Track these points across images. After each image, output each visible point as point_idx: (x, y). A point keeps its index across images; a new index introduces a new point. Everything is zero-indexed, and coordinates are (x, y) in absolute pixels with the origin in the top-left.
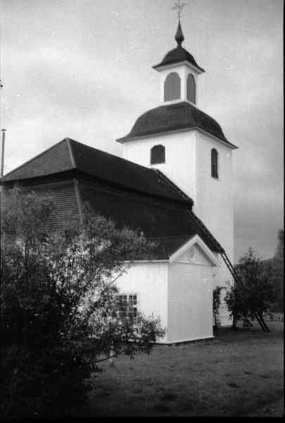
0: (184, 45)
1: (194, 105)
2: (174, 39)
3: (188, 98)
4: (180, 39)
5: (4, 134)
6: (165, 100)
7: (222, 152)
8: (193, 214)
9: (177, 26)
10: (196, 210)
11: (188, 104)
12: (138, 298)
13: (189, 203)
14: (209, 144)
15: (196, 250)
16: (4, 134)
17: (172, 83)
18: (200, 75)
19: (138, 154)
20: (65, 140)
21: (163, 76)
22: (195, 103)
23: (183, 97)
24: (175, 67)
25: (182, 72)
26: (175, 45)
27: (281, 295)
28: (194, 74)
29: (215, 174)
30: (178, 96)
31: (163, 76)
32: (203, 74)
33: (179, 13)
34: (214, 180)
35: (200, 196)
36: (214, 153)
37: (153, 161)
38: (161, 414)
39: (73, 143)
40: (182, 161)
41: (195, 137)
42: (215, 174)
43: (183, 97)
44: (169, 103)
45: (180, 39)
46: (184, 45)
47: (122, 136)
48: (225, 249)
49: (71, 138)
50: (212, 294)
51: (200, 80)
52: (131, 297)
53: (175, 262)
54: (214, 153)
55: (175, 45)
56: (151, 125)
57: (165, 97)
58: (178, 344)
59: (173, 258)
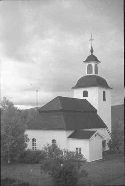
0: (94, 54)
3: (95, 73)
4: (92, 51)
5: (37, 92)
8: (97, 115)
9: (91, 47)
10: (98, 113)
11: (95, 75)
13: (96, 111)
14: (102, 90)
15: (97, 135)
16: (37, 92)
17: (90, 68)
18: (99, 64)
19: (78, 94)
20: (57, 97)
21: (86, 65)
23: (93, 73)
25: (93, 64)
28: (97, 64)
29: (104, 100)
31: (86, 65)
32: (100, 63)
33: (92, 42)
34: (105, 102)
35: (99, 107)
36: (104, 93)
38: (88, 185)
40: (94, 96)
41: (97, 89)
42: (104, 100)
43: (93, 73)
44: (88, 75)
45: (92, 51)
48: (107, 126)
49: (59, 96)
50: (102, 153)
51: (99, 66)
52: (79, 149)
53: (91, 140)
54: (104, 93)
55: (90, 54)
58: (92, 162)
59: (90, 139)
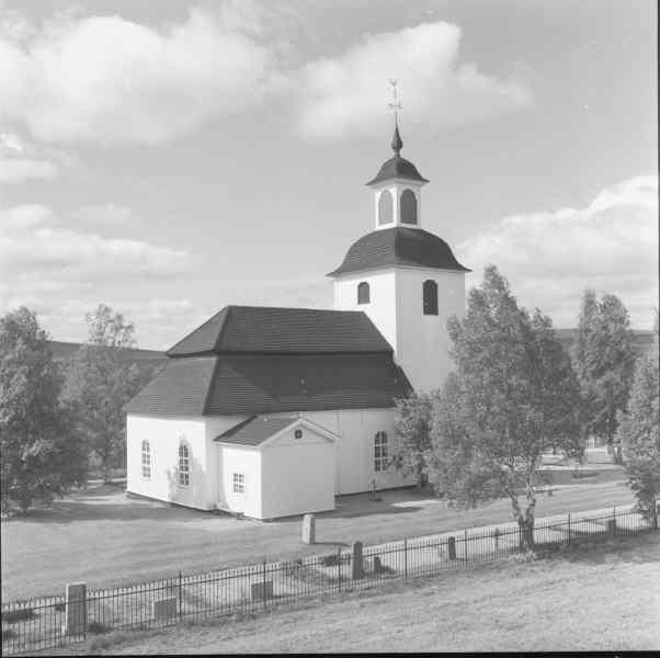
2: (390, 148)
4: (398, 145)
6: (381, 223)
19: (343, 297)
26: (392, 154)
30: (392, 221)
34: (431, 318)
55: (392, 154)
56: (363, 257)
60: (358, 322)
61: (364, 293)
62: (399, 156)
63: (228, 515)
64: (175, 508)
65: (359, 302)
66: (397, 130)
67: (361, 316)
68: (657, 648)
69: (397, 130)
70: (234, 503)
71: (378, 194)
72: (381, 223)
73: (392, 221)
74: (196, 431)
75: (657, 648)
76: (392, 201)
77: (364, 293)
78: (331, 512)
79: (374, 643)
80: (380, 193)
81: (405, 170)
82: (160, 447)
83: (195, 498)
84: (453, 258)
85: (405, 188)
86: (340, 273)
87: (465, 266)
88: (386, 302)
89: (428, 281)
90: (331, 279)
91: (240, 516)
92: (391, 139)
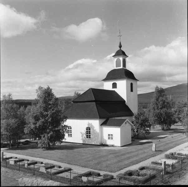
1: (125, 68)
2: (119, 47)
4: (120, 47)
6: (116, 67)
7: (133, 82)
12: (109, 134)
19: (108, 86)
20: (90, 89)
22: (125, 67)
24: (116, 81)
26: (119, 49)
27: (187, 103)
29: (132, 91)
30: (121, 67)
34: (132, 92)
36: (132, 84)
37: (113, 88)
39: (92, 89)
42: (132, 91)
43: (121, 67)
45: (120, 47)
46: (122, 49)
47: (103, 79)
54: (132, 84)
55: (119, 49)
56: (113, 75)
57: (115, 88)
60: (112, 94)
61: (115, 85)
62: (121, 49)
63: (107, 146)
64: (84, 145)
65: (113, 88)
66: (120, 42)
67: (114, 91)
68: (2, 186)
69: (120, 42)
70: (109, 142)
71: (116, 59)
72: (116, 67)
73: (121, 67)
74: (95, 123)
75: (2, 185)
76: (121, 61)
77: (115, 85)
78: (131, 144)
79: (56, 184)
80: (116, 59)
81: (123, 54)
82: (77, 129)
83: (94, 141)
84: (134, 76)
85: (124, 58)
86: (105, 80)
87: (137, 79)
88: (122, 88)
89: (114, 83)
90: (103, 82)
91: (113, 146)
92: (118, 45)
